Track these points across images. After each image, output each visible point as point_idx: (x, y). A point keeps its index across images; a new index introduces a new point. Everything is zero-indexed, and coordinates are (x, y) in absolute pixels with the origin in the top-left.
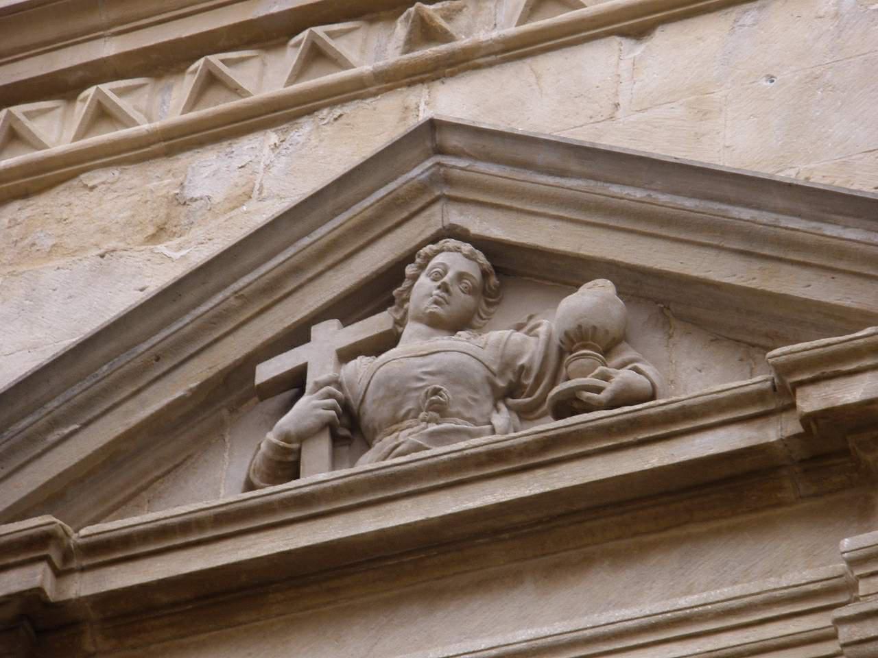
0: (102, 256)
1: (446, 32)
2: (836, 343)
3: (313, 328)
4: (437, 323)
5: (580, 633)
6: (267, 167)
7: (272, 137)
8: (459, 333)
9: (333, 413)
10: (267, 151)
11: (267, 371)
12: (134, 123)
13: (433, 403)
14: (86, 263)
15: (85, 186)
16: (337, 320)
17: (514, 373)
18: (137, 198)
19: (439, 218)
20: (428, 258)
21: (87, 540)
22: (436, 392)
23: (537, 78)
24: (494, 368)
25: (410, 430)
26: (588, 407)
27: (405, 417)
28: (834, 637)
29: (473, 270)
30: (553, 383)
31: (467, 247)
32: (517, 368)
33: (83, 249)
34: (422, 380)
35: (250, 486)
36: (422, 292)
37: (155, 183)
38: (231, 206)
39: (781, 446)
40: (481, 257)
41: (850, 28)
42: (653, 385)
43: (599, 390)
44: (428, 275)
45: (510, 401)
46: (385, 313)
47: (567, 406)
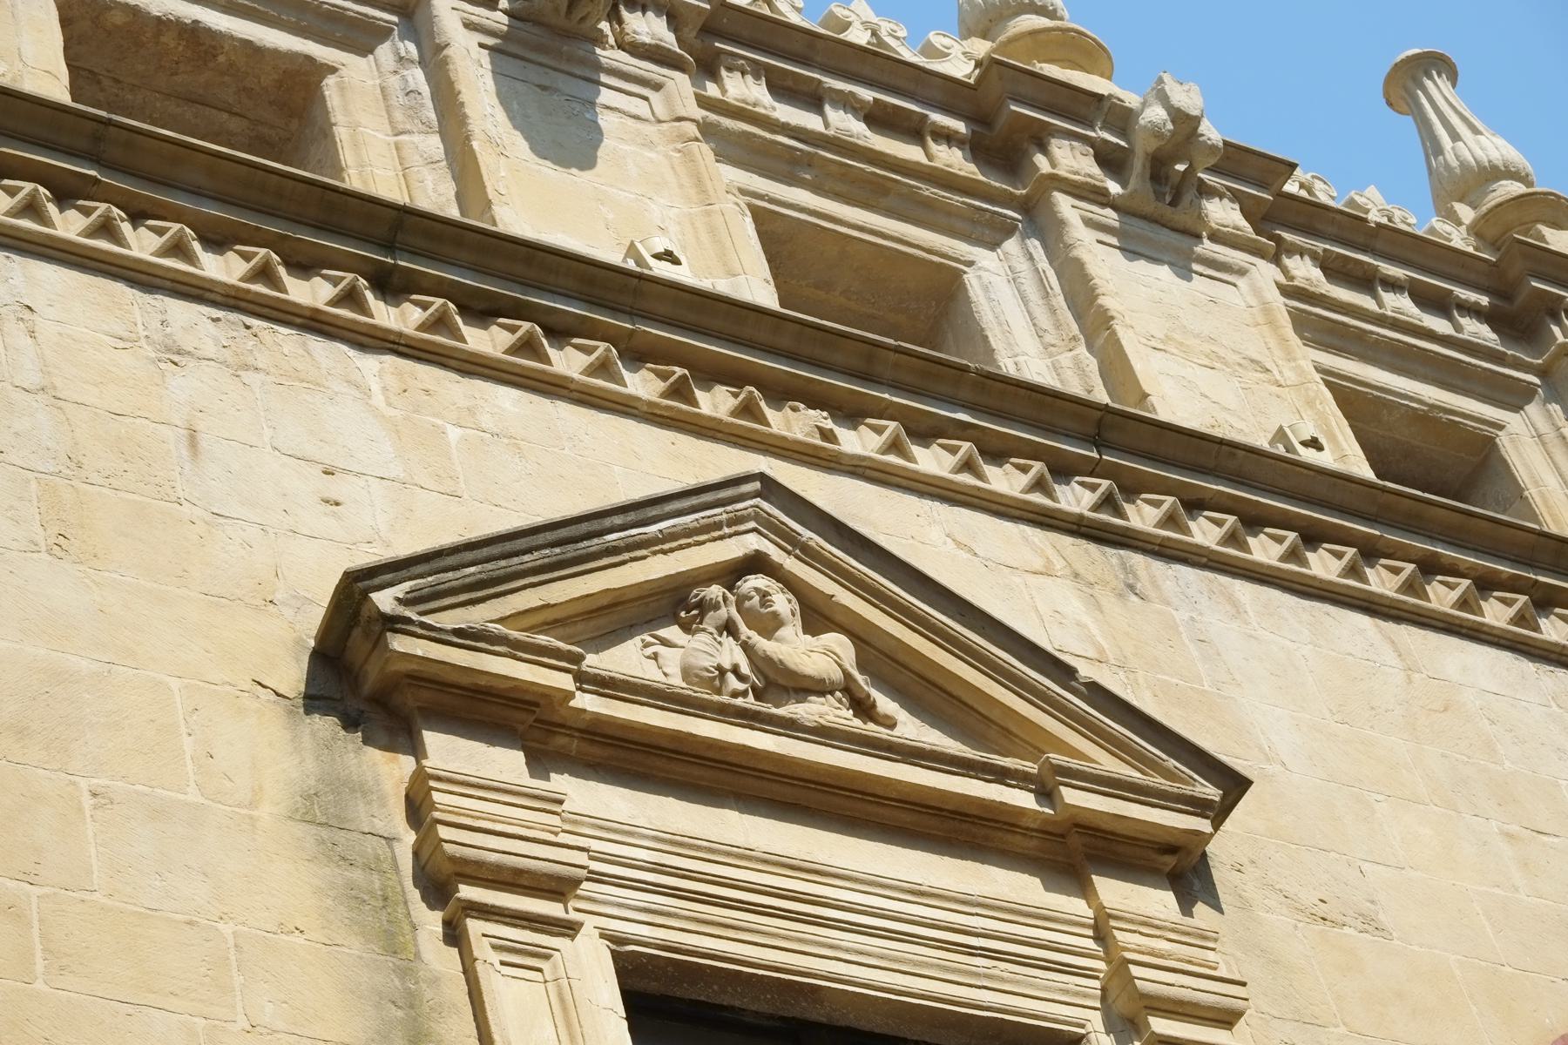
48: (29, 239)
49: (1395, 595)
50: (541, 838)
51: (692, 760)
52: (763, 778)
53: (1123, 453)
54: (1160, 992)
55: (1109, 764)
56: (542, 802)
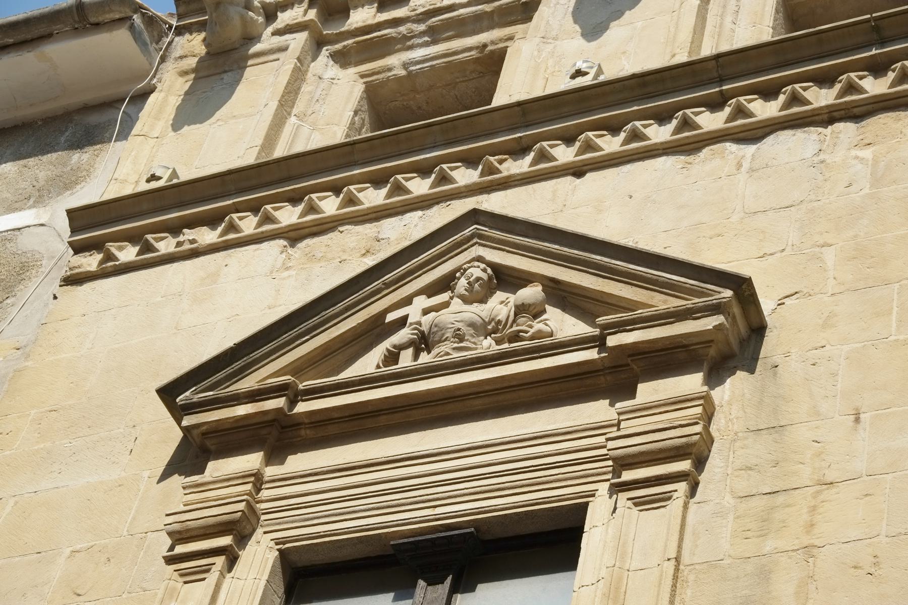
0: (340, 262)
1: (498, 169)
2: (625, 316)
3: (414, 299)
4: (466, 300)
5: (504, 439)
6: (416, 226)
7: (420, 213)
8: (474, 304)
9: (416, 337)
10: (416, 218)
11: (391, 317)
12: (363, 204)
13: (457, 334)
14: (333, 265)
15: (339, 231)
16: (425, 296)
17: (495, 323)
18: (359, 237)
19: (474, 252)
20: (465, 270)
21: (305, 387)
22: (459, 329)
23: (534, 191)
24: (487, 320)
25: (446, 346)
26: (522, 339)
27: (445, 340)
28: (605, 447)
29: (485, 276)
30: (511, 326)
31: (483, 266)
32: (497, 321)
33: (334, 258)
34: (454, 324)
35: (378, 367)
36: (462, 283)
37: (368, 231)
38: (398, 242)
39: (599, 361)
40: (489, 270)
41: (667, 176)
42: (552, 330)
43: (526, 332)
44: (465, 277)
45: (493, 335)
46: (446, 293)
47: (515, 337)
48: (609, 158)
49: (835, 101)
50: (188, 509)
51: (536, 385)
52: (413, 409)
53: (803, 63)
54: (224, 519)
55: (663, 302)
56: (626, 415)
